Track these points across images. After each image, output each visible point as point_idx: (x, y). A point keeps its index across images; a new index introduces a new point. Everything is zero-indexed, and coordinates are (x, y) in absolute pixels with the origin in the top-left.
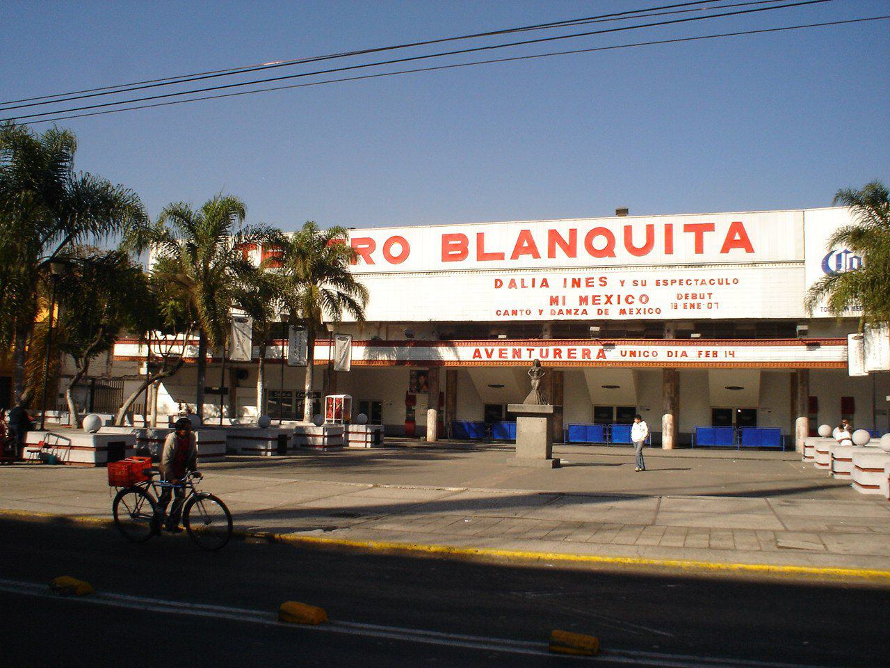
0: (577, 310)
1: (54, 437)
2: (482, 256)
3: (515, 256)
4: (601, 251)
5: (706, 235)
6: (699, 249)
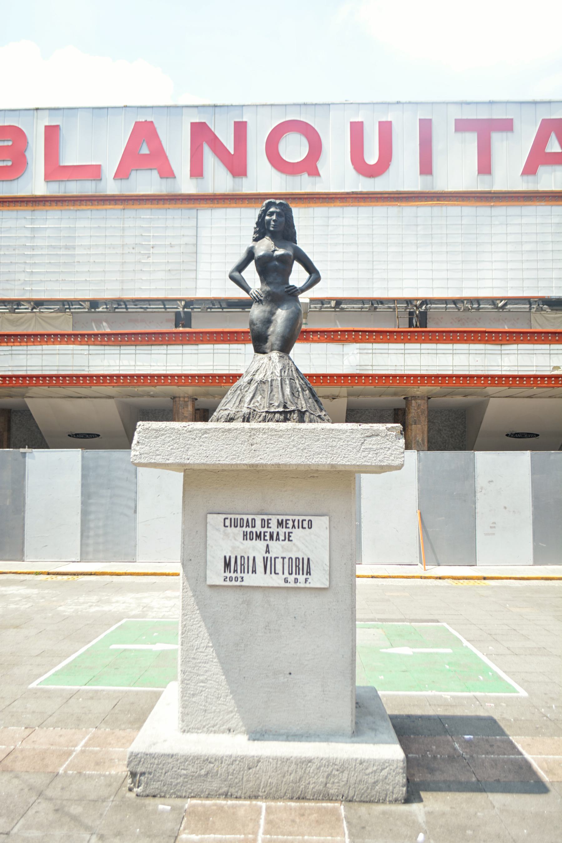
0: (294, 526)
1: (318, 585)
2: (54, 170)
3: (122, 173)
4: (363, 159)
5: (497, 138)
6: (485, 167)
